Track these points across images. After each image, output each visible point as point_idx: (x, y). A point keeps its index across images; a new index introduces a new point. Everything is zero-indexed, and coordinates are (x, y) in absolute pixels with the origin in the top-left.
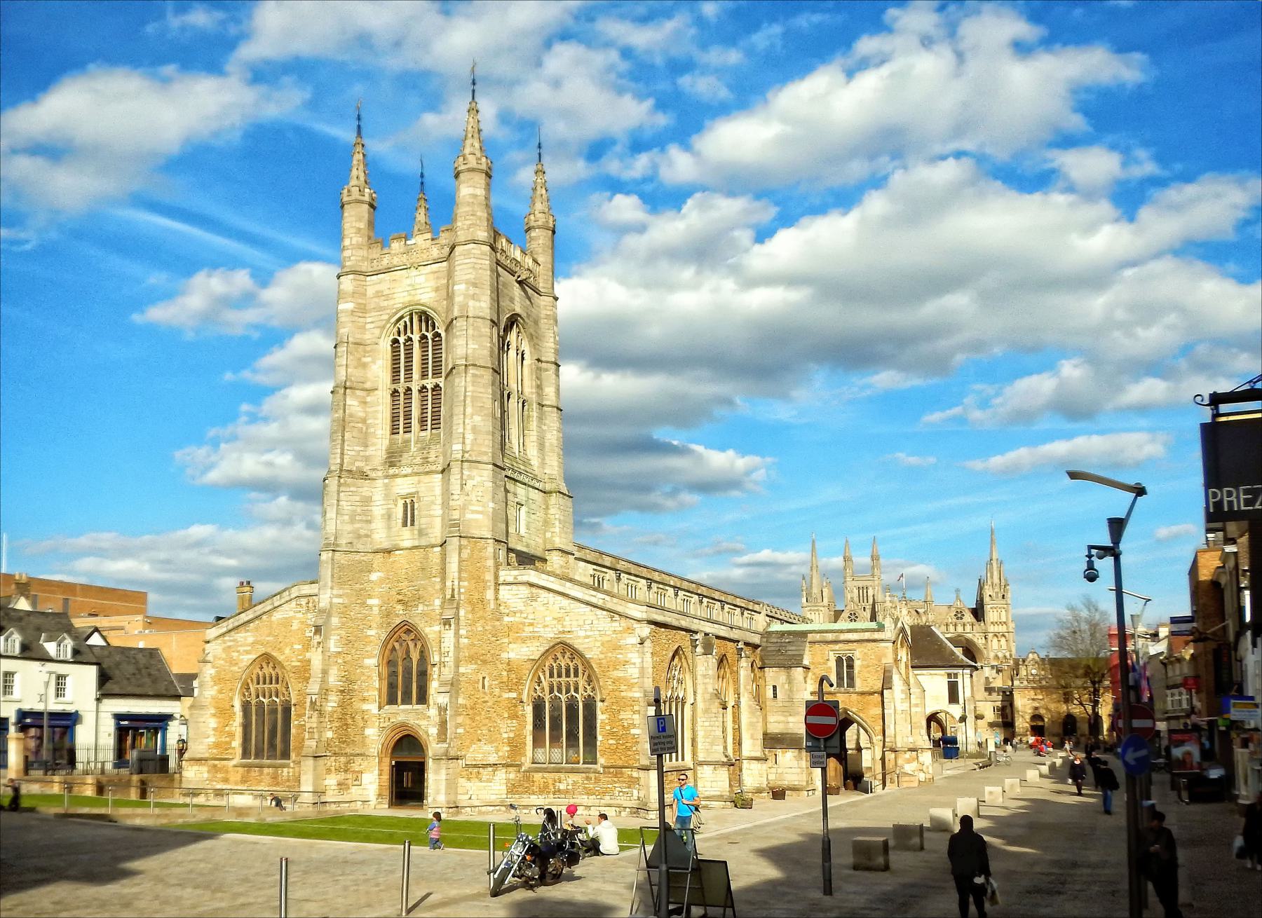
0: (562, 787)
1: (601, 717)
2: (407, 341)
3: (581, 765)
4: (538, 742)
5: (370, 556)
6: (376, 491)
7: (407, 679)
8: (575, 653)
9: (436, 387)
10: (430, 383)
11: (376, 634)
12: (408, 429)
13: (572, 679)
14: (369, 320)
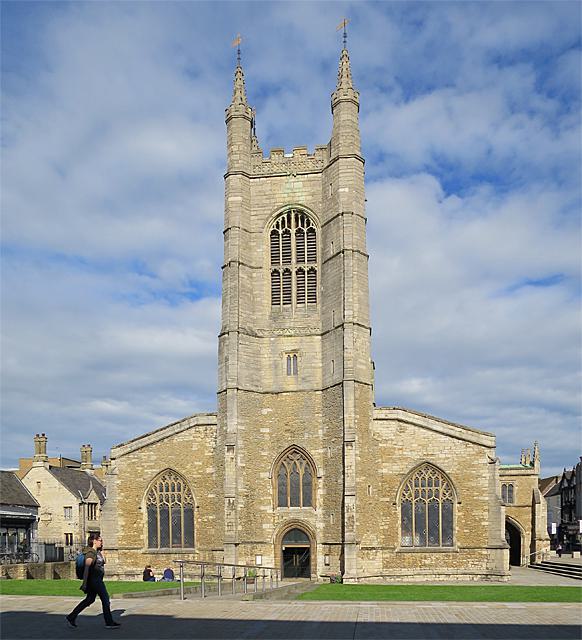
0: (427, 562)
1: (457, 514)
2: (284, 233)
3: (441, 547)
4: (406, 529)
5: (262, 396)
6: (265, 347)
7: (295, 491)
8: (436, 469)
9: (312, 270)
10: (306, 267)
11: (268, 455)
12: (288, 301)
13: (434, 488)
14: (253, 213)
